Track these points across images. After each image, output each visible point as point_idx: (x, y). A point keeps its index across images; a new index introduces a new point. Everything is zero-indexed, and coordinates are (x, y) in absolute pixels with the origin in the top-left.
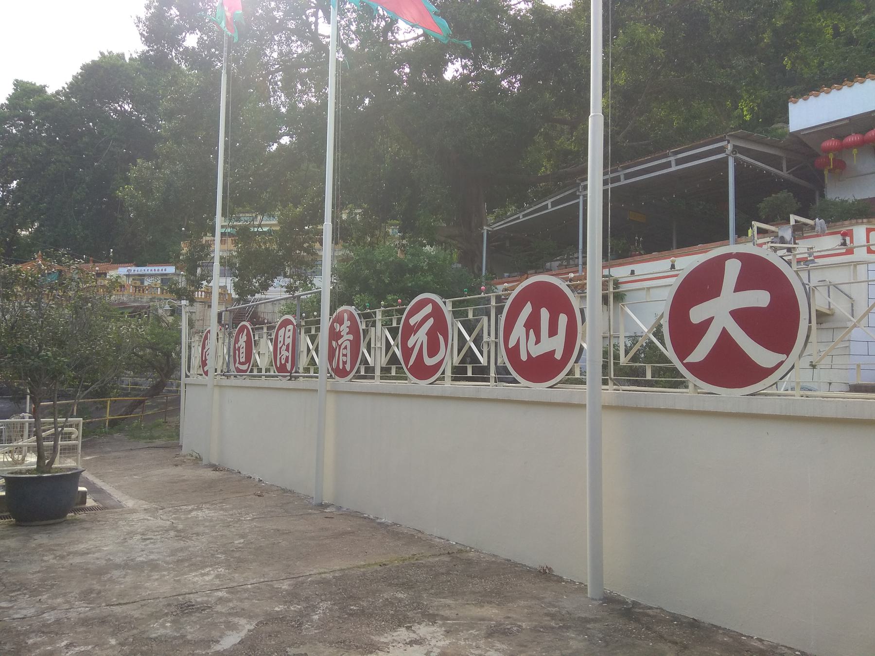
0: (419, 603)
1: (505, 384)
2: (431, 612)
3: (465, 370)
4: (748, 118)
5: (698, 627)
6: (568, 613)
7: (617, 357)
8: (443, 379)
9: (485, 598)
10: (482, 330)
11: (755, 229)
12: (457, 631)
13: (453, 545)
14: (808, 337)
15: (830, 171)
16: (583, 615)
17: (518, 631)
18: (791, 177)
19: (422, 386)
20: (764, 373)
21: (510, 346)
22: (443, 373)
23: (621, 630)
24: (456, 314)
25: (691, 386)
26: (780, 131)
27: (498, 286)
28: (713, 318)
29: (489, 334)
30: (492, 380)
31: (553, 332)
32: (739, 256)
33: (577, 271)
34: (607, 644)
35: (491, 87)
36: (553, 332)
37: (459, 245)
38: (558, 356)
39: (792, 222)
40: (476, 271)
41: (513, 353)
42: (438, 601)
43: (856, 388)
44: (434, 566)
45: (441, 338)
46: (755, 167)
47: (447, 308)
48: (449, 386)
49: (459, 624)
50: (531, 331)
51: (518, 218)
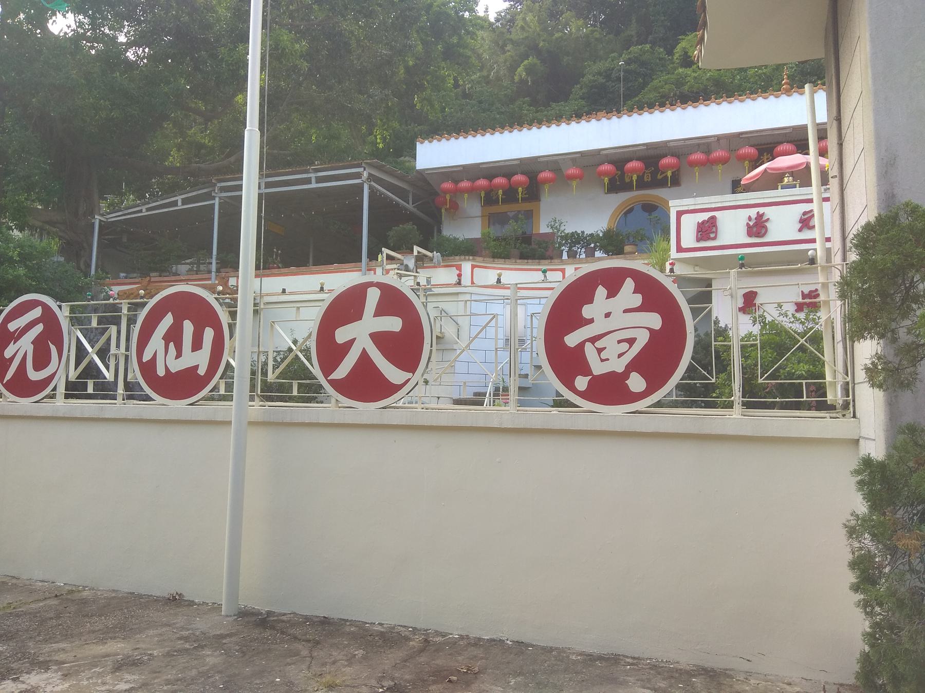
0: (24, 654)
1: (135, 402)
2: (41, 659)
3: (85, 386)
4: (381, 146)
5: (329, 623)
6: (203, 633)
7: (265, 373)
8: (52, 396)
9: (107, 635)
10: (109, 339)
11: (385, 255)
12: (77, 673)
13: (60, 587)
14: (429, 358)
15: (446, 210)
16: (218, 633)
17: (149, 660)
18: (415, 210)
19: (25, 404)
20: (390, 389)
21: (145, 359)
22: (55, 389)
23: (257, 638)
24: (75, 321)
25: (333, 401)
26: (407, 164)
27: (113, 288)
28: (353, 341)
29: (118, 346)
30: (120, 398)
31: (197, 345)
32: (378, 285)
33: (210, 279)
34: (244, 654)
35: (112, 57)
36: (197, 345)
37: (61, 234)
38: (202, 371)
39: (415, 253)
40: (82, 266)
41: (148, 369)
42: (46, 648)
43: (458, 402)
44: (39, 612)
45: (53, 348)
46: (387, 197)
47: (63, 314)
48: (61, 404)
49: (79, 666)
50: (172, 345)
51: (141, 211)
